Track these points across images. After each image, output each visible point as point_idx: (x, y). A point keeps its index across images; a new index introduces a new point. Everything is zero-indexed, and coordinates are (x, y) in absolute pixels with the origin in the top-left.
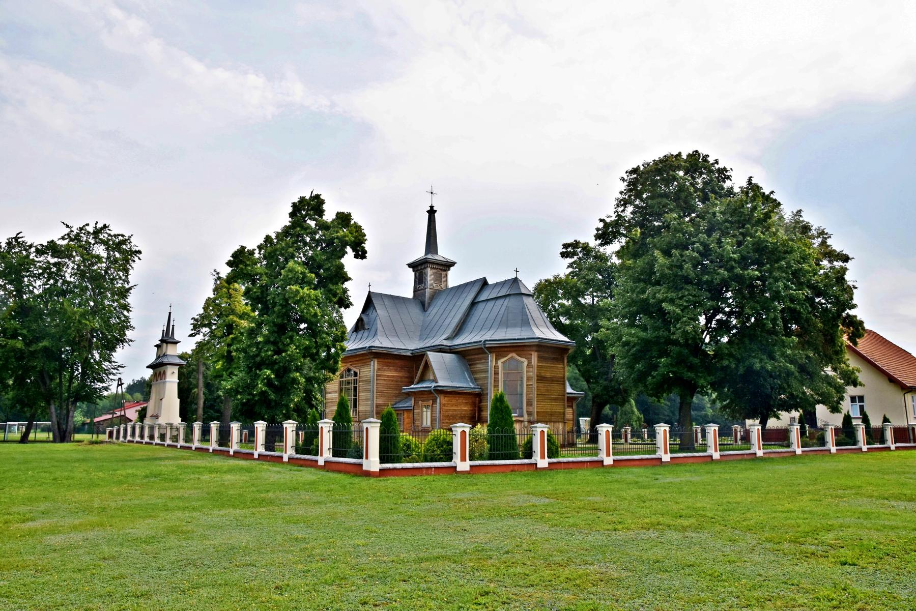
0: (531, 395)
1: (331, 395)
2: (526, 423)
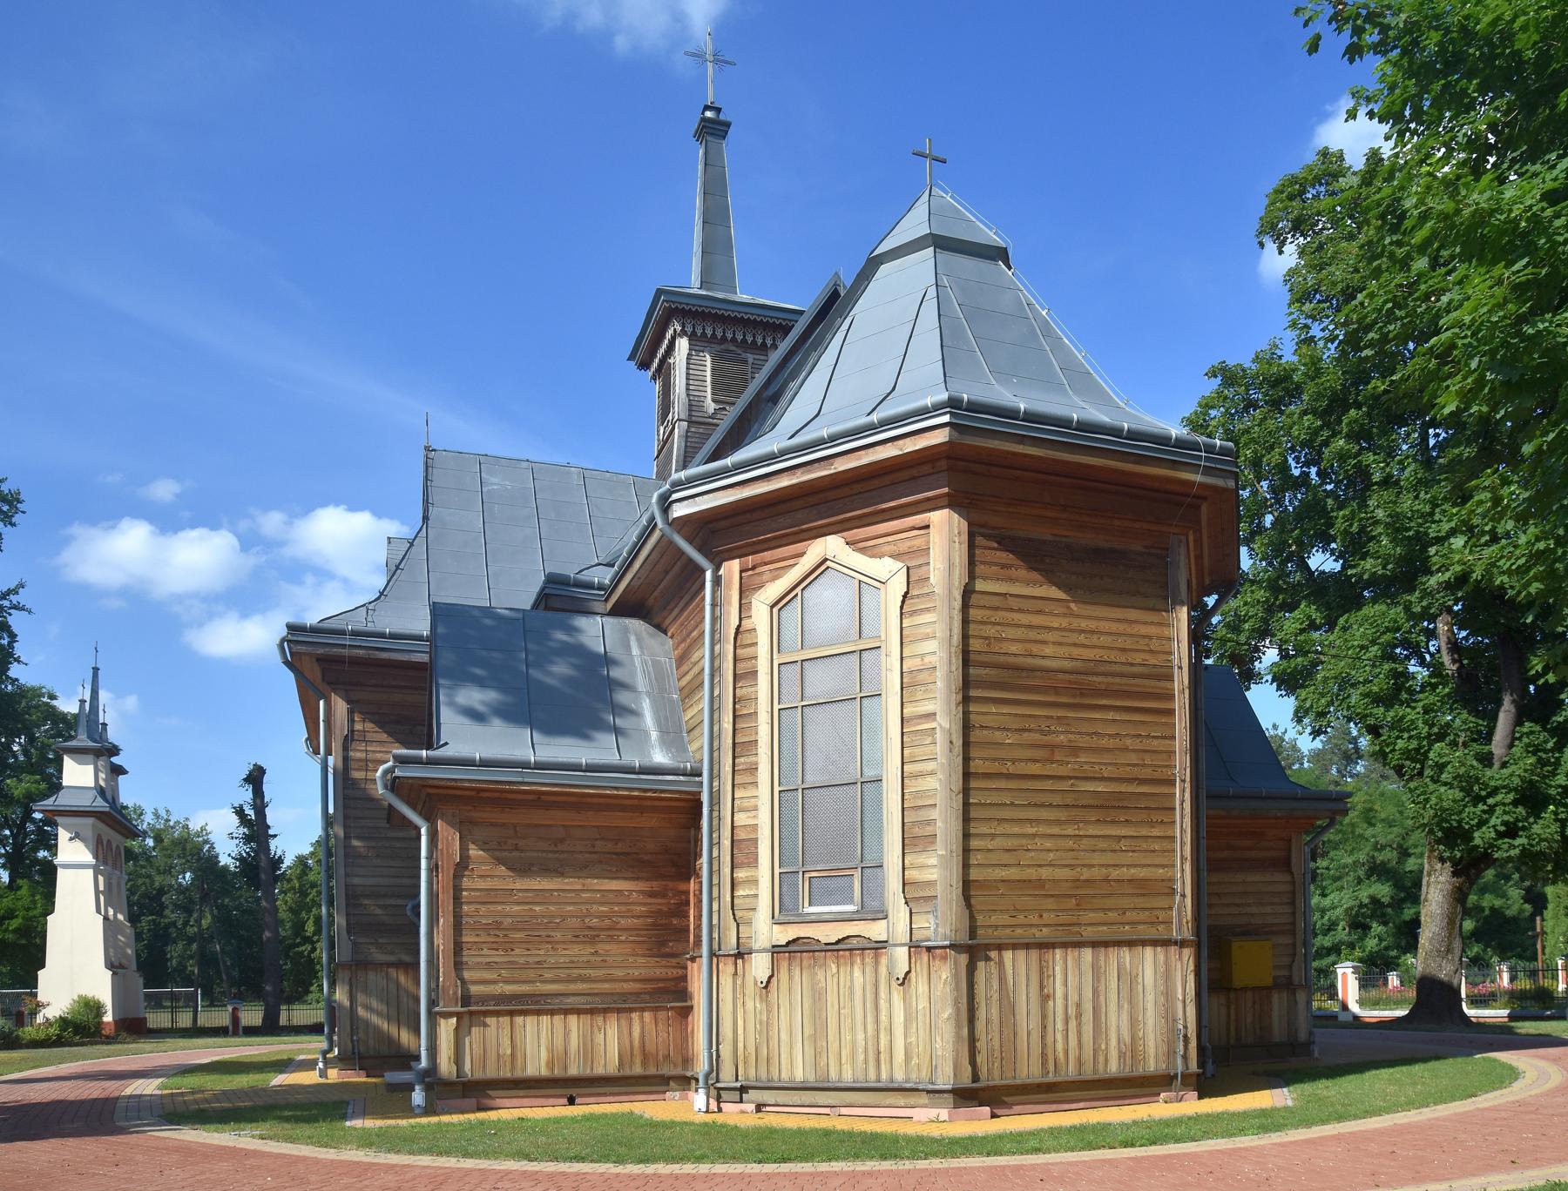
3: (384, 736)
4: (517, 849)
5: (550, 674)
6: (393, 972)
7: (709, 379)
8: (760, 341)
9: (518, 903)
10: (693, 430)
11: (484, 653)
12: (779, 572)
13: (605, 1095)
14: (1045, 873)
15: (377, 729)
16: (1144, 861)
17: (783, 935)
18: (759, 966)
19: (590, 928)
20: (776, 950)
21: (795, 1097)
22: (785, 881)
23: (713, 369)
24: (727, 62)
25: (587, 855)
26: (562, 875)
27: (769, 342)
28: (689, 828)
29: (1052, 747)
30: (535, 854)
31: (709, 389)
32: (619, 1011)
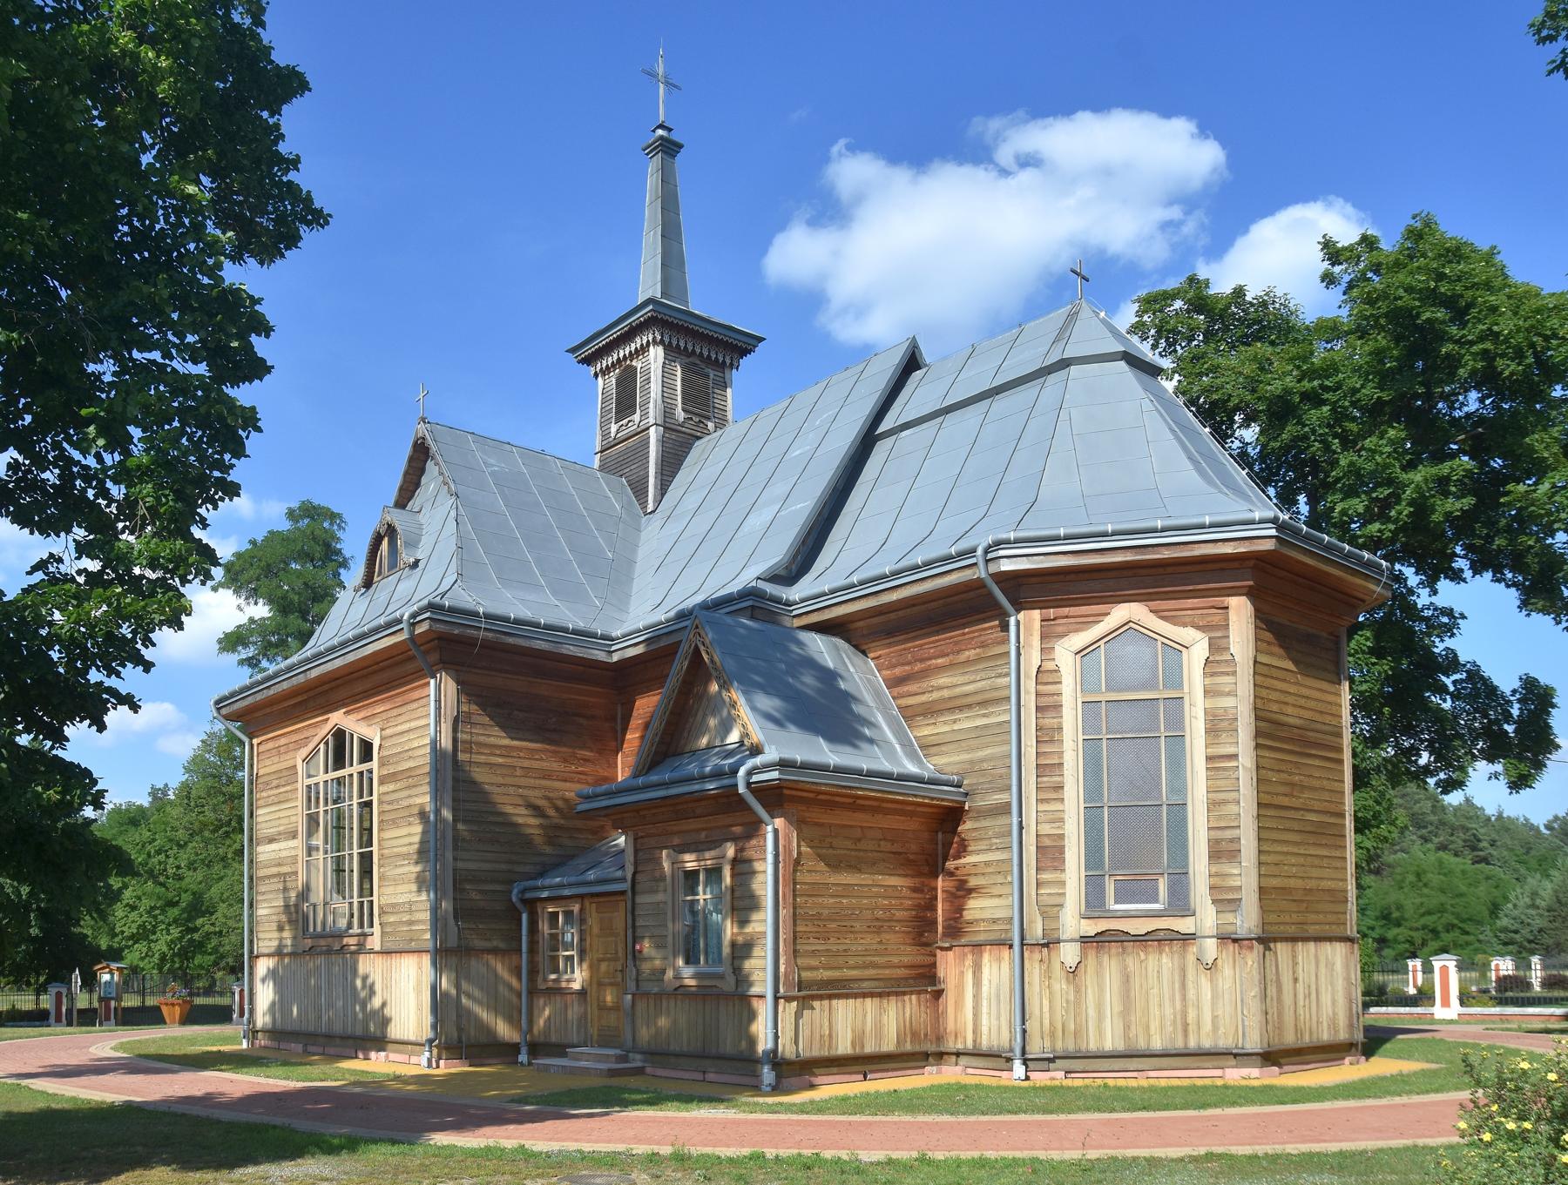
0: (1232, 809)
1: (274, 846)
2: (1211, 945)
3: (486, 720)
4: (831, 847)
5: (803, 683)
6: (491, 959)
7: (679, 388)
8: (721, 359)
9: (832, 896)
10: (667, 435)
11: (752, 661)
12: (1081, 626)
13: (887, 1070)
14: (1292, 883)
15: (480, 712)
16: (1334, 876)
17: (1091, 928)
18: (1069, 954)
19: (877, 919)
20: (1085, 940)
21: (1106, 1064)
22: (1094, 888)
23: (683, 380)
24: (675, 86)
25: (875, 854)
26: (860, 871)
27: (728, 361)
28: (937, 832)
29: (1292, 785)
30: (842, 852)
31: (679, 398)
32: (897, 994)
